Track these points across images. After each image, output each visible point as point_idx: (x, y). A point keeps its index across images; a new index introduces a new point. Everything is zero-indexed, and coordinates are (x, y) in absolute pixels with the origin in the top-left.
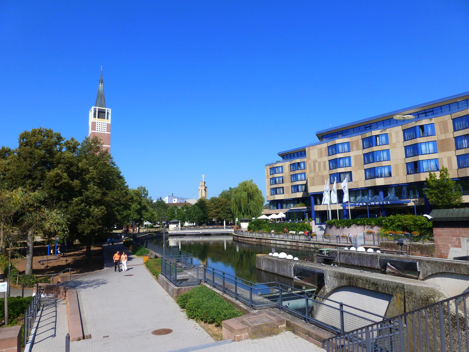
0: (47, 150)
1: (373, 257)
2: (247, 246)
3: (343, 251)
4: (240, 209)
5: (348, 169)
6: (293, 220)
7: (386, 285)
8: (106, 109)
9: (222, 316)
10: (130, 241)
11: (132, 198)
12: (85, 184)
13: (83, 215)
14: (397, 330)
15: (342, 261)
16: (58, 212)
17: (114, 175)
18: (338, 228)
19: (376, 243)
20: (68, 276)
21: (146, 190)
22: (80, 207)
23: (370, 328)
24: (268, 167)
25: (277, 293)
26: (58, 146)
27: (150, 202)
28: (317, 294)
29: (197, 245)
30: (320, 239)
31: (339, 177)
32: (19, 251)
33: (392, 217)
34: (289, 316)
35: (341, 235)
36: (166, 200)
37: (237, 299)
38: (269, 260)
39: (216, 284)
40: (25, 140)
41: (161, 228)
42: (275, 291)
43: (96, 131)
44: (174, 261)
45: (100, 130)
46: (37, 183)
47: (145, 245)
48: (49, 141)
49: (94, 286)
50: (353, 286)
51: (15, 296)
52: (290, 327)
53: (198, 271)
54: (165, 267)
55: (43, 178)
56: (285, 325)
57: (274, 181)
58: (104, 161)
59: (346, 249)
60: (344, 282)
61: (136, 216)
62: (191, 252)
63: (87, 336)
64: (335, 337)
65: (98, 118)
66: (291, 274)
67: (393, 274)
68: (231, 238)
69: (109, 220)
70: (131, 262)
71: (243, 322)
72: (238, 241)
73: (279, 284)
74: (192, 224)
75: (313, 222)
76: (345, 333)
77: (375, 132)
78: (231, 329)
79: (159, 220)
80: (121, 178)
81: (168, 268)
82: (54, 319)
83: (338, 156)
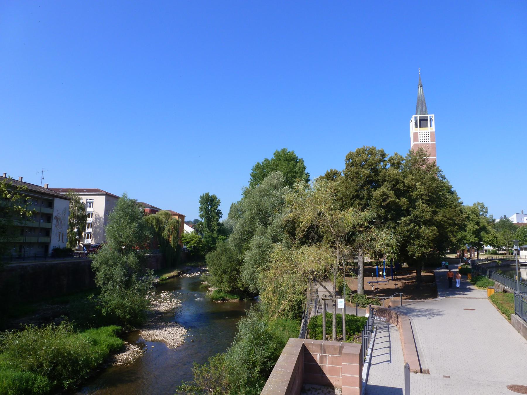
0: (372, 168)
8: (429, 116)
12: (412, 202)
13: (413, 236)
16: (387, 232)
17: (443, 190)
21: (485, 206)
22: (408, 228)
26: (382, 163)
27: (491, 222)
36: (514, 219)
41: (508, 255)
43: (419, 143)
45: (423, 140)
46: (364, 203)
47: (488, 274)
48: (373, 159)
49: (428, 316)
51: (350, 314)
55: (370, 198)
58: (432, 174)
61: (473, 239)
63: (425, 371)
65: (420, 127)
69: (441, 242)
80: (452, 193)
82: (388, 344)
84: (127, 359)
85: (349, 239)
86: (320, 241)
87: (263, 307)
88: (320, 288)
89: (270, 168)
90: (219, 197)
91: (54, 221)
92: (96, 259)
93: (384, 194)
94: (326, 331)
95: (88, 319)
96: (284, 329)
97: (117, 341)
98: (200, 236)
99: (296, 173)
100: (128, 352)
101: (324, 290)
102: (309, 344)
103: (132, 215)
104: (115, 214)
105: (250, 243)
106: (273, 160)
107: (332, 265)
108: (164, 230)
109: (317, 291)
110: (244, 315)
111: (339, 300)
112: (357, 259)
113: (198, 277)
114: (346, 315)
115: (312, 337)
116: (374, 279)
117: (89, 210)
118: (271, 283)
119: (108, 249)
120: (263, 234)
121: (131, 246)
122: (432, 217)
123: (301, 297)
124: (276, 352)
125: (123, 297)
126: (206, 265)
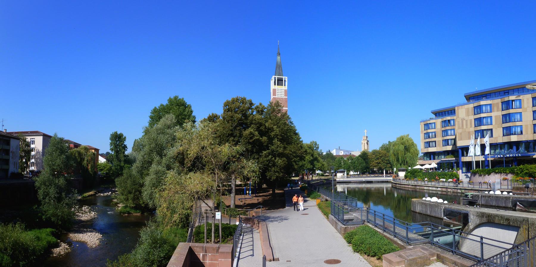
1: (507, 198)
2: (404, 192)
3: (484, 194)
4: (398, 160)
5: (489, 127)
6: (443, 169)
7: (516, 219)
8: (284, 77)
9: (382, 251)
10: (305, 186)
11: (306, 151)
12: (271, 140)
13: (270, 165)
14: (522, 253)
15: (483, 203)
18: (480, 175)
19: (510, 187)
20: (260, 211)
22: (268, 159)
23: (503, 254)
24: (423, 123)
25: (429, 231)
26: (250, 110)
27: (320, 155)
28: (462, 230)
29: (361, 191)
30: (466, 185)
31: (482, 134)
32: (228, 190)
33: (521, 166)
34: (439, 249)
35: (482, 181)
36: (334, 152)
37: (395, 236)
38: (423, 203)
39: (377, 224)
40: (227, 107)
42: (428, 230)
44: (341, 204)
48: (244, 107)
50: (491, 222)
52: (440, 259)
53: (362, 213)
54: (334, 209)
55: (241, 136)
56: (435, 258)
57: (427, 135)
59: (487, 192)
60: (485, 220)
61: (309, 166)
62: (356, 197)
64: (477, 264)
66: (441, 215)
67: (521, 211)
68: (390, 185)
69: (289, 169)
70: (306, 204)
71: (400, 256)
72: (396, 188)
73: (431, 222)
74: (356, 173)
75: (461, 171)
76: (484, 260)
77: (512, 98)
78: (390, 262)
79: (328, 169)
80: (296, 134)
81: (337, 210)
83: (482, 115)
84: (60, 253)
85: (225, 167)
86: (203, 169)
87: (159, 219)
88: (203, 205)
89: (165, 112)
90: (124, 135)
91: (11, 154)
92: (38, 181)
93: (251, 133)
94: (207, 236)
95: (33, 222)
96: (176, 236)
97: (53, 239)
98: (111, 165)
99: (185, 116)
100: (61, 248)
101: (206, 206)
102: (194, 247)
103: (61, 150)
104: (49, 149)
105: (149, 170)
106: (167, 105)
107: (212, 187)
108: (84, 160)
109: (200, 207)
110: (145, 225)
111: (217, 213)
112: (231, 182)
113: (110, 196)
114: (222, 224)
115: (197, 241)
116: (243, 196)
117: (32, 146)
118: (165, 201)
119: (46, 174)
120: (159, 163)
121: (61, 172)
122: (284, 151)
123: (189, 211)
124: (169, 253)
125: (57, 209)
126: (115, 187)
